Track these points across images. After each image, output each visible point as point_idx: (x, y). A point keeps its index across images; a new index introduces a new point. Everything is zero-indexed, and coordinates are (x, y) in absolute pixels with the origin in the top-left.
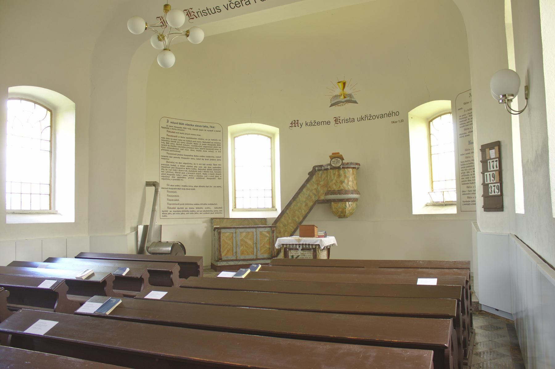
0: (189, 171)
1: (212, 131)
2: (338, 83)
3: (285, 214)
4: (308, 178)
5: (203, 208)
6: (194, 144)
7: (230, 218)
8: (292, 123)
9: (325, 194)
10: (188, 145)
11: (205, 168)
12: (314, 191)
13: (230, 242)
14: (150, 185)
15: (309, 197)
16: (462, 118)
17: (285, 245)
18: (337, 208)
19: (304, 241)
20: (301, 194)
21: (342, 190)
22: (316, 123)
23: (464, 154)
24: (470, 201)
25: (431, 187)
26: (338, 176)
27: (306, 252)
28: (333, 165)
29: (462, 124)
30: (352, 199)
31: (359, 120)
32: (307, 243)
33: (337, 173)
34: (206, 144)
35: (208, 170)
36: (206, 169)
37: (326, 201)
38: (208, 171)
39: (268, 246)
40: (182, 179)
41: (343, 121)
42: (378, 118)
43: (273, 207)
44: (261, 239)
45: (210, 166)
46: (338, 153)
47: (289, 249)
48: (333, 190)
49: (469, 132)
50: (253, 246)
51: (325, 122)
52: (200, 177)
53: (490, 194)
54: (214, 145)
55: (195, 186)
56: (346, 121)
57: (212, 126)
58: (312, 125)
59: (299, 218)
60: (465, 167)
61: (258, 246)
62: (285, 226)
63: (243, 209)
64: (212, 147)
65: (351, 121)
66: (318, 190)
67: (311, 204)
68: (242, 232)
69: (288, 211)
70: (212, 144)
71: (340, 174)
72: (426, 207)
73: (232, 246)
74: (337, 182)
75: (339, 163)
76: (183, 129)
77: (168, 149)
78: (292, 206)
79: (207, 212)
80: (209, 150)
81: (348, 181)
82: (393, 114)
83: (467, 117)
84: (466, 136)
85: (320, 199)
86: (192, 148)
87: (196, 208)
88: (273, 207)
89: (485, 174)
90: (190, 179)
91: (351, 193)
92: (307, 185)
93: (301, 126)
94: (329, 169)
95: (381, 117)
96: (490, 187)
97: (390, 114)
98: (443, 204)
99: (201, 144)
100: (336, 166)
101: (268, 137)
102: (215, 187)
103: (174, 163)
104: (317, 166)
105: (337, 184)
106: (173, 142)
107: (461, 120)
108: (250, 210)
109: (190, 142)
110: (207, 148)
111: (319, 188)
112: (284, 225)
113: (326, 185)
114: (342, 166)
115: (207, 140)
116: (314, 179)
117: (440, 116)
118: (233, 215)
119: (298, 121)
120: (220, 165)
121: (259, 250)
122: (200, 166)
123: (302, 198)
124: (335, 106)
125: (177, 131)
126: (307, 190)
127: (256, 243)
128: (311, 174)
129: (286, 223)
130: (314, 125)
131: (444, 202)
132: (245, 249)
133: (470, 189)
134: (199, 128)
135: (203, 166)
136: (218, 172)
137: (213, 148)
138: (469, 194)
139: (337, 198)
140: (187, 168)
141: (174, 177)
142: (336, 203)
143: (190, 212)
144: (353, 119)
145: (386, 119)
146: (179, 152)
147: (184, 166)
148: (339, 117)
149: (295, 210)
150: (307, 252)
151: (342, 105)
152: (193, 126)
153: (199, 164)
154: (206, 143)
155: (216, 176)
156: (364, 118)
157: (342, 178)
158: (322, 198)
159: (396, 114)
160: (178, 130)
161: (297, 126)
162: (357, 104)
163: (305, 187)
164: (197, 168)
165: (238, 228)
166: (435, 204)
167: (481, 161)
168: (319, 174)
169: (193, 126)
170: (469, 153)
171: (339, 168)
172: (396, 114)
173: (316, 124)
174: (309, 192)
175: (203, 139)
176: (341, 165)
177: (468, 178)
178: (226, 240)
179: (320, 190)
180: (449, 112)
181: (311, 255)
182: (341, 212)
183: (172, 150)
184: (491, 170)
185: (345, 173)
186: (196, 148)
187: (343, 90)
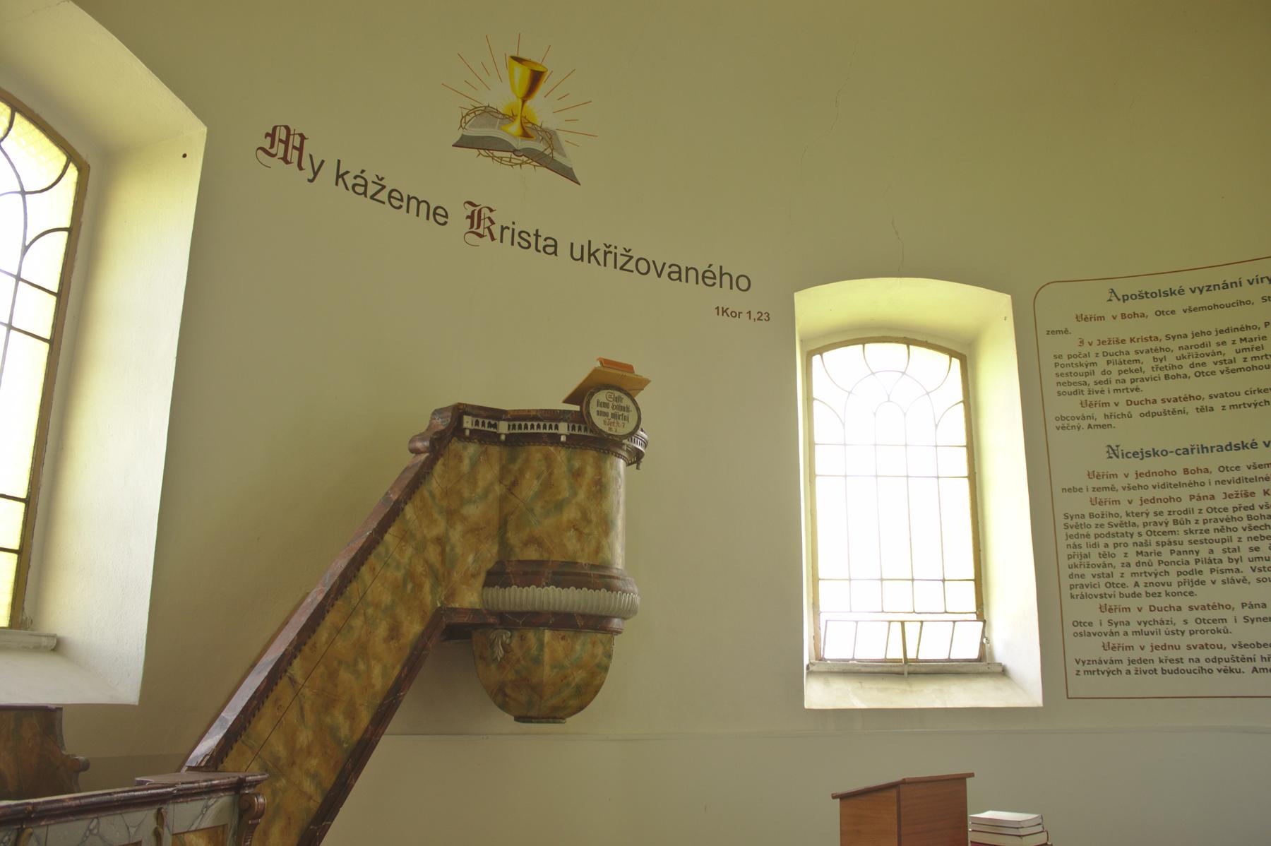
2: (515, 63)
8: (272, 135)
12: (432, 553)
15: (410, 586)
18: (567, 663)
23: (1080, 490)
24: (1120, 661)
28: (599, 422)
41: (507, 233)
42: (659, 276)
46: (629, 368)
48: (557, 557)
51: (423, 207)
56: (517, 239)
58: (365, 193)
59: (351, 715)
60: (1088, 536)
65: (540, 248)
68: (184, 833)
71: (603, 480)
74: (589, 522)
75: (626, 419)
78: (323, 635)
83: (1094, 364)
92: (403, 509)
93: (316, 174)
94: (563, 439)
98: (897, 670)
104: (473, 407)
111: (456, 535)
124: (475, 152)
126: (405, 537)
129: (280, 749)
133: (1117, 617)
138: (1112, 634)
142: (563, 638)
144: (552, 243)
145: (691, 288)
148: (491, 210)
149: (335, 663)
156: (600, 255)
159: (741, 283)
162: (578, 185)
163: (394, 521)
168: (460, 459)
172: (741, 283)
173: (383, 196)
179: (459, 550)
180: (902, 336)
182: (578, 687)
187: (524, 102)
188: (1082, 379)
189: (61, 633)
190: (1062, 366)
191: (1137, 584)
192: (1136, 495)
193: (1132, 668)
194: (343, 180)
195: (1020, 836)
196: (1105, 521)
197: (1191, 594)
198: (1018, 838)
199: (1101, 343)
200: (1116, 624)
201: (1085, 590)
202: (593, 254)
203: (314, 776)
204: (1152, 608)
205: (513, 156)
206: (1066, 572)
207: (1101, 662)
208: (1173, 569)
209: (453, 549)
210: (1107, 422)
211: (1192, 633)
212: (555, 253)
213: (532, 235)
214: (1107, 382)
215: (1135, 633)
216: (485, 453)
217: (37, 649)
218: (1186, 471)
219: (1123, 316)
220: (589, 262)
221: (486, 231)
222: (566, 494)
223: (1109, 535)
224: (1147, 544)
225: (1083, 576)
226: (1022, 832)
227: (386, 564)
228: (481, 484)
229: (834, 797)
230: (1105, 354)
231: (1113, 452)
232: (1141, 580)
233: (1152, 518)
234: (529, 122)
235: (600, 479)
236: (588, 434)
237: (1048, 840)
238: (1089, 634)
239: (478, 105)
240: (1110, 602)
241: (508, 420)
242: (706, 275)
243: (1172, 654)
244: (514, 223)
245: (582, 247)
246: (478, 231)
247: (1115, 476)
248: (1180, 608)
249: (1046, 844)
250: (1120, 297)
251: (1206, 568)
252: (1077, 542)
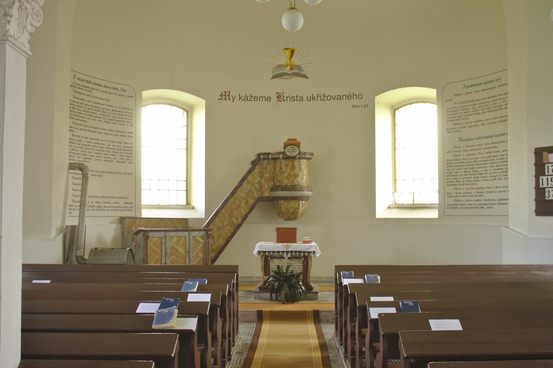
0: (96, 150)
1: (123, 95)
2: (286, 50)
3: (220, 214)
4: (251, 168)
5: (110, 203)
6: (102, 111)
7: (142, 217)
8: (221, 95)
9: (270, 189)
10: (95, 114)
11: (113, 147)
12: (257, 186)
13: (158, 250)
14: (73, 168)
15: (250, 193)
16: (451, 111)
17: (267, 253)
19: (294, 248)
20: (240, 188)
21: (296, 185)
22: (253, 98)
23: (451, 152)
24: (458, 205)
25: (394, 187)
26: (291, 168)
27: (293, 261)
28: (288, 154)
29: (451, 118)
30: (306, 197)
31: (309, 99)
32: (298, 250)
33: (290, 164)
34: (115, 114)
35: (117, 149)
36: (115, 149)
37: (271, 199)
38: (117, 151)
39: (201, 256)
40: (88, 160)
41: (288, 99)
42: (334, 100)
43: (188, 203)
44: (194, 246)
45: (120, 145)
46: (295, 140)
47: (270, 257)
48: (283, 184)
49: (460, 128)
50: (186, 255)
51: (264, 98)
52: (108, 159)
53: (547, 199)
54: (125, 115)
55: (102, 172)
56: (291, 99)
57: (124, 89)
58: (247, 100)
59: (237, 219)
60: (452, 166)
61: (191, 256)
62: (219, 229)
63: (150, 205)
64: (122, 118)
65: (298, 100)
66: (261, 184)
67: (252, 202)
69: (223, 210)
70: (123, 114)
72: (389, 210)
73: (160, 255)
74: (290, 176)
75: (296, 152)
76: (91, 90)
77: (74, 117)
78: (229, 204)
79: (116, 209)
80: (120, 123)
81: (303, 175)
82: (355, 96)
83: (458, 110)
84: (455, 131)
85: (264, 196)
86: (99, 118)
87: (104, 203)
88: (188, 203)
89: (541, 177)
90: (97, 161)
91: (306, 190)
92: (247, 178)
93: (234, 100)
95: (338, 99)
96: (548, 191)
97: (350, 96)
98: (412, 207)
99: (109, 113)
100: (292, 155)
101: (184, 110)
102: (126, 174)
103: (80, 137)
104: (262, 153)
105: (290, 178)
106: (79, 107)
107: (449, 113)
108: (159, 207)
109: (97, 109)
110: (117, 119)
111: (263, 181)
112: (218, 228)
113: (273, 178)
114: (298, 156)
115: (117, 107)
116: (257, 170)
117: (410, 104)
118: (146, 214)
119: (229, 92)
120: (132, 144)
121: (192, 260)
122: (108, 144)
123: (241, 193)
124: (277, 78)
125: (84, 92)
127: (189, 252)
128: (254, 163)
129: (221, 226)
130: (249, 100)
131: (413, 204)
132: (176, 259)
133: (458, 191)
134: (108, 90)
135: (112, 144)
136: (130, 154)
137: (124, 120)
138: (457, 196)
139: (289, 196)
140: (93, 146)
141: (80, 158)
142: (287, 202)
143: (96, 208)
145: (344, 101)
146: (86, 121)
147: (90, 143)
148: (283, 93)
150: (295, 261)
151: (288, 78)
152: (102, 86)
153: (108, 141)
154: (115, 112)
155: (126, 159)
156: (316, 98)
157: (296, 171)
158: (267, 194)
159: (359, 97)
160: (85, 90)
161: (228, 100)
163: (245, 180)
164: (105, 147)
165: (168, 231)
166: (401, 206)
167: (534, 164)
169: (102, 86)
170: (459, 151)
171: (294, 158)
172: (359, 97)
173: (252, 99)
174: (250, 186)
175: (113, 107)
176: (297, 155)
177: (457, 179)
178: (153, 248)
179: (263, 184)
181: (299, 264)
183: (78, 118)
184: (550, 174)
185: (300, 165)
186: (104, 118)
187: (290, 60)
188: (454, 116)
189: (194, 206)
190: (449, 112)
191: (463, 181)
192: (465, 153)
193: (461, 207)
194: (241, 99)
196: (457, 162)
197: (476, 184)
199: (460, 103)
200: (458, 193)
201: (451, 183)
202: (314, 98)
203: (229, 230)
204: (467, 189)
205: (289, 76)
206: (446, 178)
207: (453, 205)
208: (472, 176)
209: (262, 184)
210: (460, 130)
211: (475, 196)
212: (302, 100)
213: (295, 97)
214: (461, 116)
215: (462, 196)
216: (269, 162)
217: (190, 208)
218: (478, 145)
219: (467, 93)
220: (313, 100)
221: (282, 100)
222: (284, 170)
223: (458, 166)
224: (467, 169)
225: (450, 179)
227: (244, 189)
228: (268, 169)
230: (461, 107)
231: (461, 139)
232: (465, 180)
233: (469, 160)
234: (292, 65)
235: (293, 166)
236: (285, 156)
238: (451, 197)
239: (277, 65)
240: (457, 187)
241: (271, 155)
242: (349, 96)
243: (470, 203)
244: (290, 95)
245: (310, 97)
246: (280, 100)
247: (460, 147)
248: (473, 189)
250: (466, 87)
251: (480, 176)
252: (449, 168)
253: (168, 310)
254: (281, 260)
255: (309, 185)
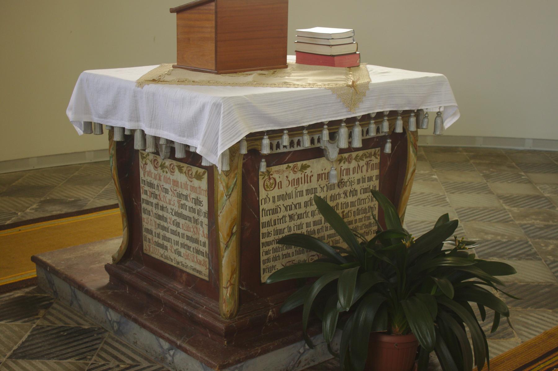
195: (329, 45)
198: (328, 47)
226: (332, 42)
229: (172, 11)
237: (357, 50)
245: (262, 204)
249: (355, 53)
253: (162, 145)
254: (305, 162)
255: (50, 310)
